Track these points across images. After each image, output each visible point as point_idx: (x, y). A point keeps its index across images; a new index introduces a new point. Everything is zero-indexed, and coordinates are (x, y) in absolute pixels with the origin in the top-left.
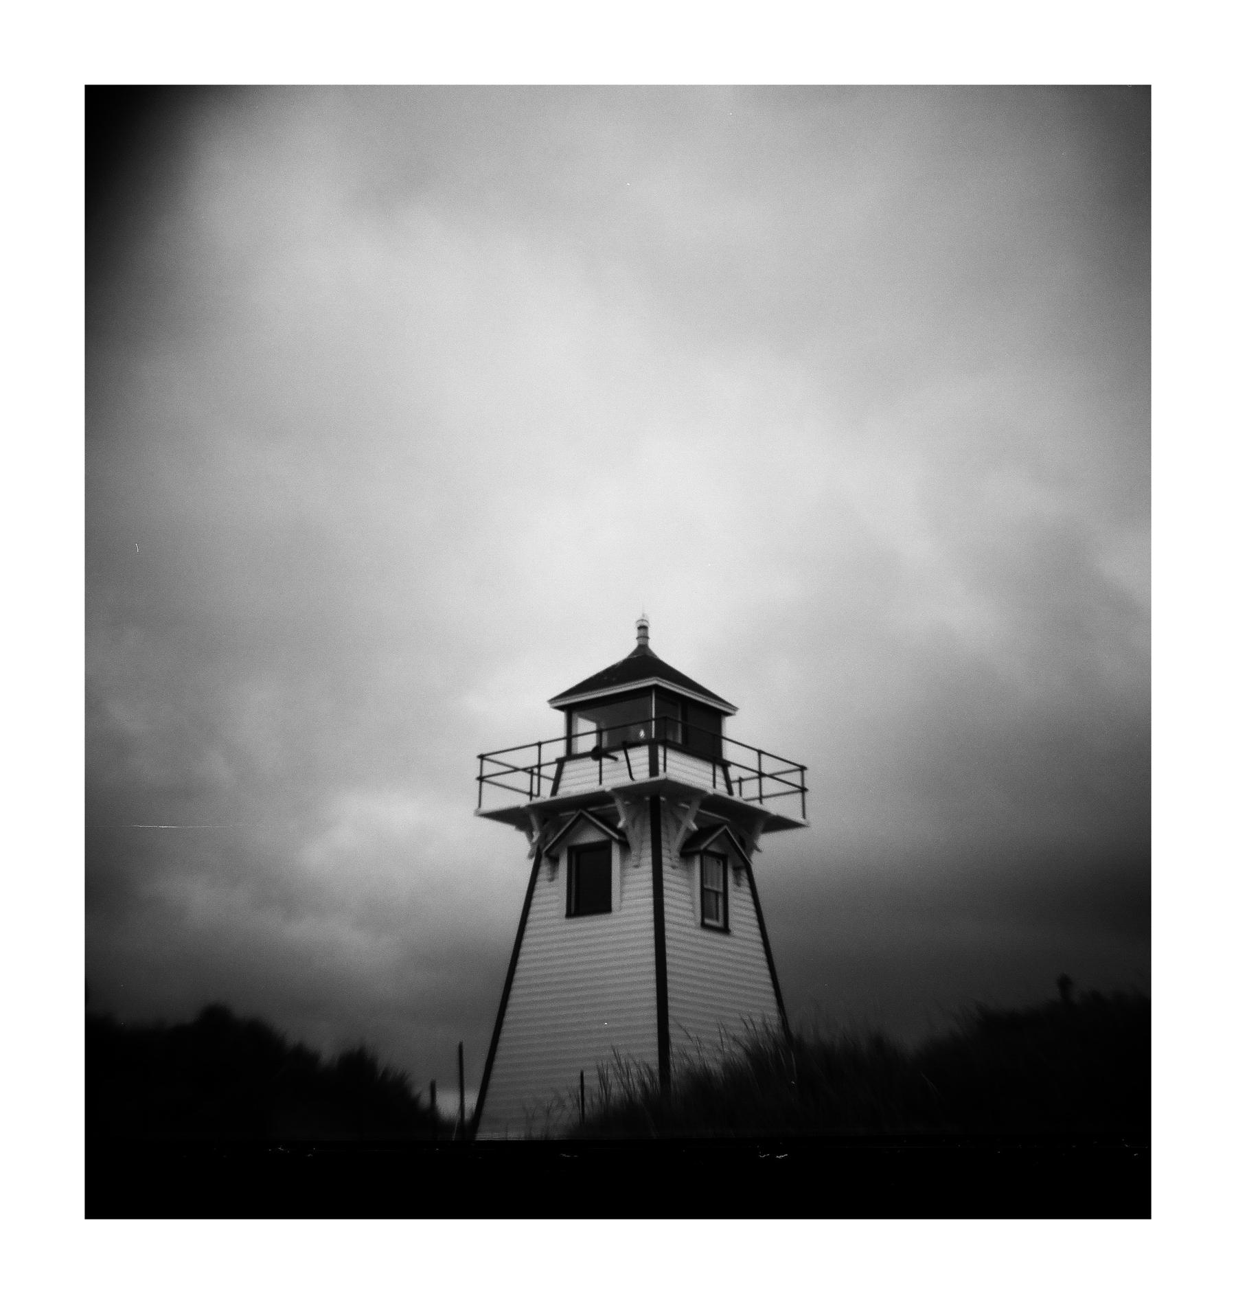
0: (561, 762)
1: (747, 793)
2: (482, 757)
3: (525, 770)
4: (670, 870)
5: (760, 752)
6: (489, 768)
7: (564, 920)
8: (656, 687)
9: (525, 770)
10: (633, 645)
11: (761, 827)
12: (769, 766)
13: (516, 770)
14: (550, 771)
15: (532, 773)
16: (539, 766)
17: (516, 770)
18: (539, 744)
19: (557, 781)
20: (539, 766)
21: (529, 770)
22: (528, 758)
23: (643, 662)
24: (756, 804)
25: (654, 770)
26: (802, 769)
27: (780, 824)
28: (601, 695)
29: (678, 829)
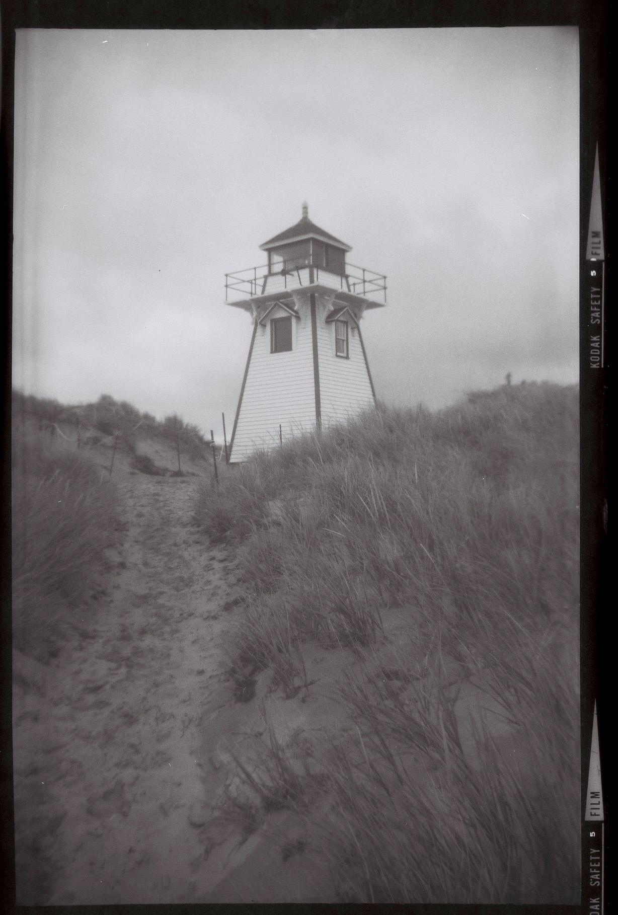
0: (266, 277)
1: (357, 291)
2: (227, 275)
8: (313, 239)
12: (368, 277)
13: (244, 281)
14: (261, 282)
17: (244, 281)
18: (255, 269)
19: (264, 286)
22: (250, 275)
23: (305, 226)
25: (312, 281)
26: (385, 277)
27: (373, 305)
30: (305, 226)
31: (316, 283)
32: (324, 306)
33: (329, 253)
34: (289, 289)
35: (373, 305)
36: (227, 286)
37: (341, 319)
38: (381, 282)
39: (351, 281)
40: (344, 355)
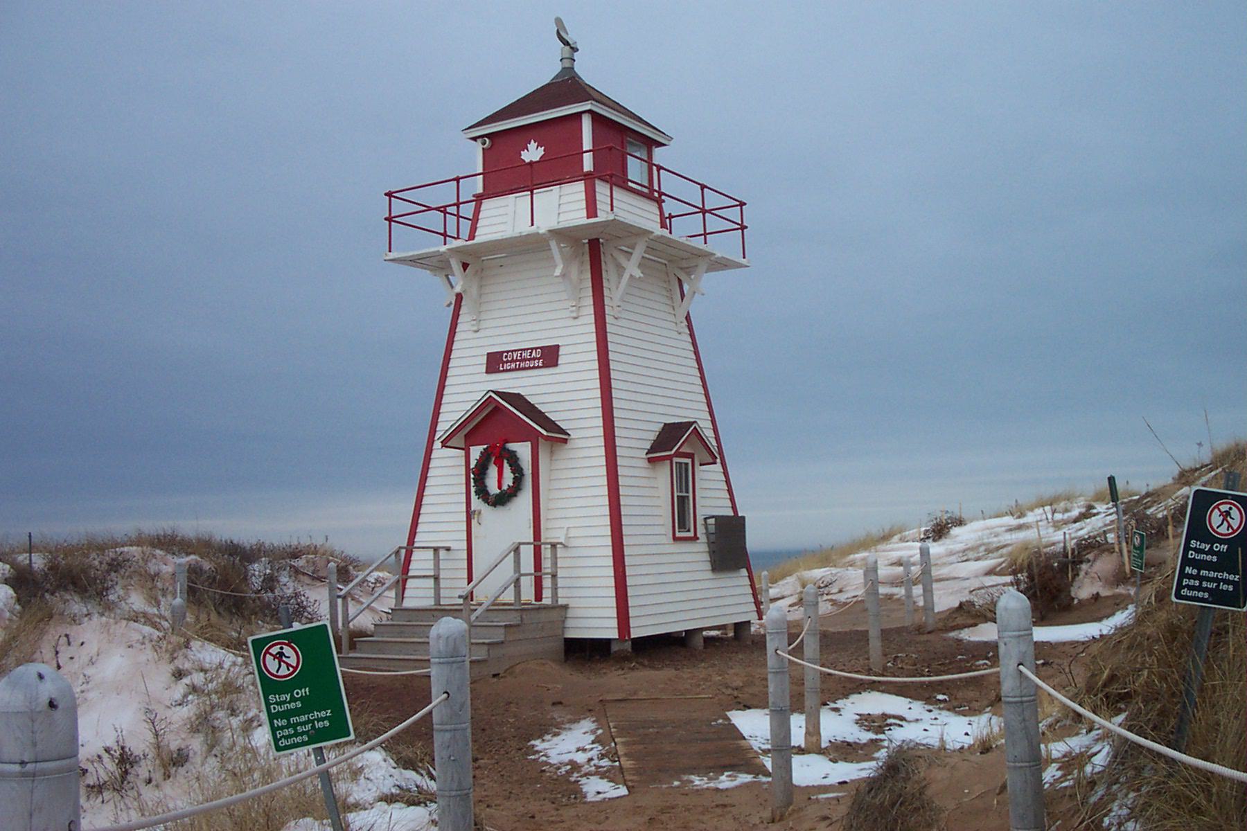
0: (479, 199)
1: (684, 229)
2: (389, 194)
3: (437, 209)
4: (614, 321)
5: (703, 187)
6: (399, 207)
7: (710, 575)
8: (589, 111)
9: (437, 209)
10: (557, 68)
11: (705, 267)
12: (712, 201)
13: (430, 209)
14: (467, 210)
15: (445, 213)
16: (458, 205)
17: (430, 209)
18: (457, 180)
19: (475, 221)
20: (458, 205)
21: (443, 210)
22: (446, 195)
23: (568, 87)
24: (698, 243)
25: (592, 210)
26: (742, 204)
27: (723, 264)
28: (613, 118)
29: (620, 276)
30: (568, 87)
31: (603, 215)
32: (620, 269)
33: (623, 143)
34: (544, 224)
35: (723, 264)
36: (390, 219)
37: (684, 450)
38: (734, 214)
39: (670, 207)
40: (691, 534)
